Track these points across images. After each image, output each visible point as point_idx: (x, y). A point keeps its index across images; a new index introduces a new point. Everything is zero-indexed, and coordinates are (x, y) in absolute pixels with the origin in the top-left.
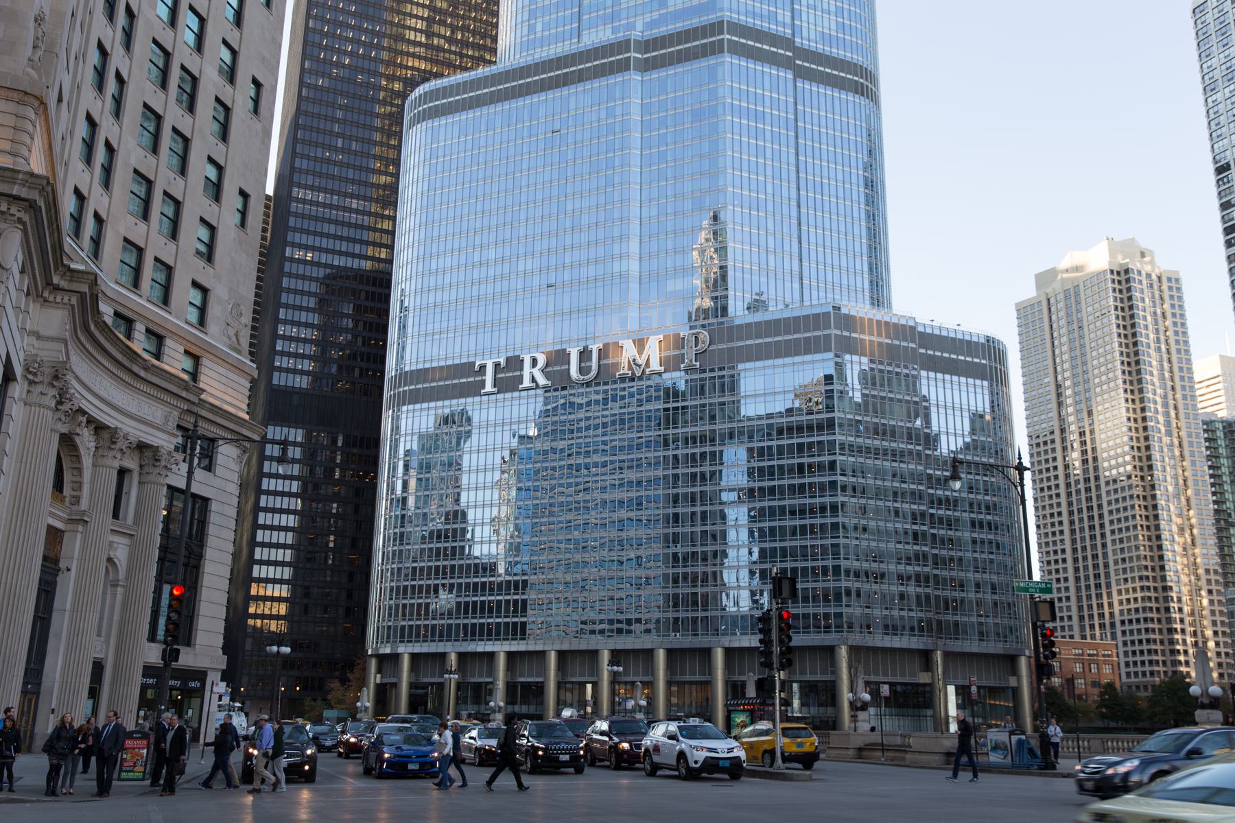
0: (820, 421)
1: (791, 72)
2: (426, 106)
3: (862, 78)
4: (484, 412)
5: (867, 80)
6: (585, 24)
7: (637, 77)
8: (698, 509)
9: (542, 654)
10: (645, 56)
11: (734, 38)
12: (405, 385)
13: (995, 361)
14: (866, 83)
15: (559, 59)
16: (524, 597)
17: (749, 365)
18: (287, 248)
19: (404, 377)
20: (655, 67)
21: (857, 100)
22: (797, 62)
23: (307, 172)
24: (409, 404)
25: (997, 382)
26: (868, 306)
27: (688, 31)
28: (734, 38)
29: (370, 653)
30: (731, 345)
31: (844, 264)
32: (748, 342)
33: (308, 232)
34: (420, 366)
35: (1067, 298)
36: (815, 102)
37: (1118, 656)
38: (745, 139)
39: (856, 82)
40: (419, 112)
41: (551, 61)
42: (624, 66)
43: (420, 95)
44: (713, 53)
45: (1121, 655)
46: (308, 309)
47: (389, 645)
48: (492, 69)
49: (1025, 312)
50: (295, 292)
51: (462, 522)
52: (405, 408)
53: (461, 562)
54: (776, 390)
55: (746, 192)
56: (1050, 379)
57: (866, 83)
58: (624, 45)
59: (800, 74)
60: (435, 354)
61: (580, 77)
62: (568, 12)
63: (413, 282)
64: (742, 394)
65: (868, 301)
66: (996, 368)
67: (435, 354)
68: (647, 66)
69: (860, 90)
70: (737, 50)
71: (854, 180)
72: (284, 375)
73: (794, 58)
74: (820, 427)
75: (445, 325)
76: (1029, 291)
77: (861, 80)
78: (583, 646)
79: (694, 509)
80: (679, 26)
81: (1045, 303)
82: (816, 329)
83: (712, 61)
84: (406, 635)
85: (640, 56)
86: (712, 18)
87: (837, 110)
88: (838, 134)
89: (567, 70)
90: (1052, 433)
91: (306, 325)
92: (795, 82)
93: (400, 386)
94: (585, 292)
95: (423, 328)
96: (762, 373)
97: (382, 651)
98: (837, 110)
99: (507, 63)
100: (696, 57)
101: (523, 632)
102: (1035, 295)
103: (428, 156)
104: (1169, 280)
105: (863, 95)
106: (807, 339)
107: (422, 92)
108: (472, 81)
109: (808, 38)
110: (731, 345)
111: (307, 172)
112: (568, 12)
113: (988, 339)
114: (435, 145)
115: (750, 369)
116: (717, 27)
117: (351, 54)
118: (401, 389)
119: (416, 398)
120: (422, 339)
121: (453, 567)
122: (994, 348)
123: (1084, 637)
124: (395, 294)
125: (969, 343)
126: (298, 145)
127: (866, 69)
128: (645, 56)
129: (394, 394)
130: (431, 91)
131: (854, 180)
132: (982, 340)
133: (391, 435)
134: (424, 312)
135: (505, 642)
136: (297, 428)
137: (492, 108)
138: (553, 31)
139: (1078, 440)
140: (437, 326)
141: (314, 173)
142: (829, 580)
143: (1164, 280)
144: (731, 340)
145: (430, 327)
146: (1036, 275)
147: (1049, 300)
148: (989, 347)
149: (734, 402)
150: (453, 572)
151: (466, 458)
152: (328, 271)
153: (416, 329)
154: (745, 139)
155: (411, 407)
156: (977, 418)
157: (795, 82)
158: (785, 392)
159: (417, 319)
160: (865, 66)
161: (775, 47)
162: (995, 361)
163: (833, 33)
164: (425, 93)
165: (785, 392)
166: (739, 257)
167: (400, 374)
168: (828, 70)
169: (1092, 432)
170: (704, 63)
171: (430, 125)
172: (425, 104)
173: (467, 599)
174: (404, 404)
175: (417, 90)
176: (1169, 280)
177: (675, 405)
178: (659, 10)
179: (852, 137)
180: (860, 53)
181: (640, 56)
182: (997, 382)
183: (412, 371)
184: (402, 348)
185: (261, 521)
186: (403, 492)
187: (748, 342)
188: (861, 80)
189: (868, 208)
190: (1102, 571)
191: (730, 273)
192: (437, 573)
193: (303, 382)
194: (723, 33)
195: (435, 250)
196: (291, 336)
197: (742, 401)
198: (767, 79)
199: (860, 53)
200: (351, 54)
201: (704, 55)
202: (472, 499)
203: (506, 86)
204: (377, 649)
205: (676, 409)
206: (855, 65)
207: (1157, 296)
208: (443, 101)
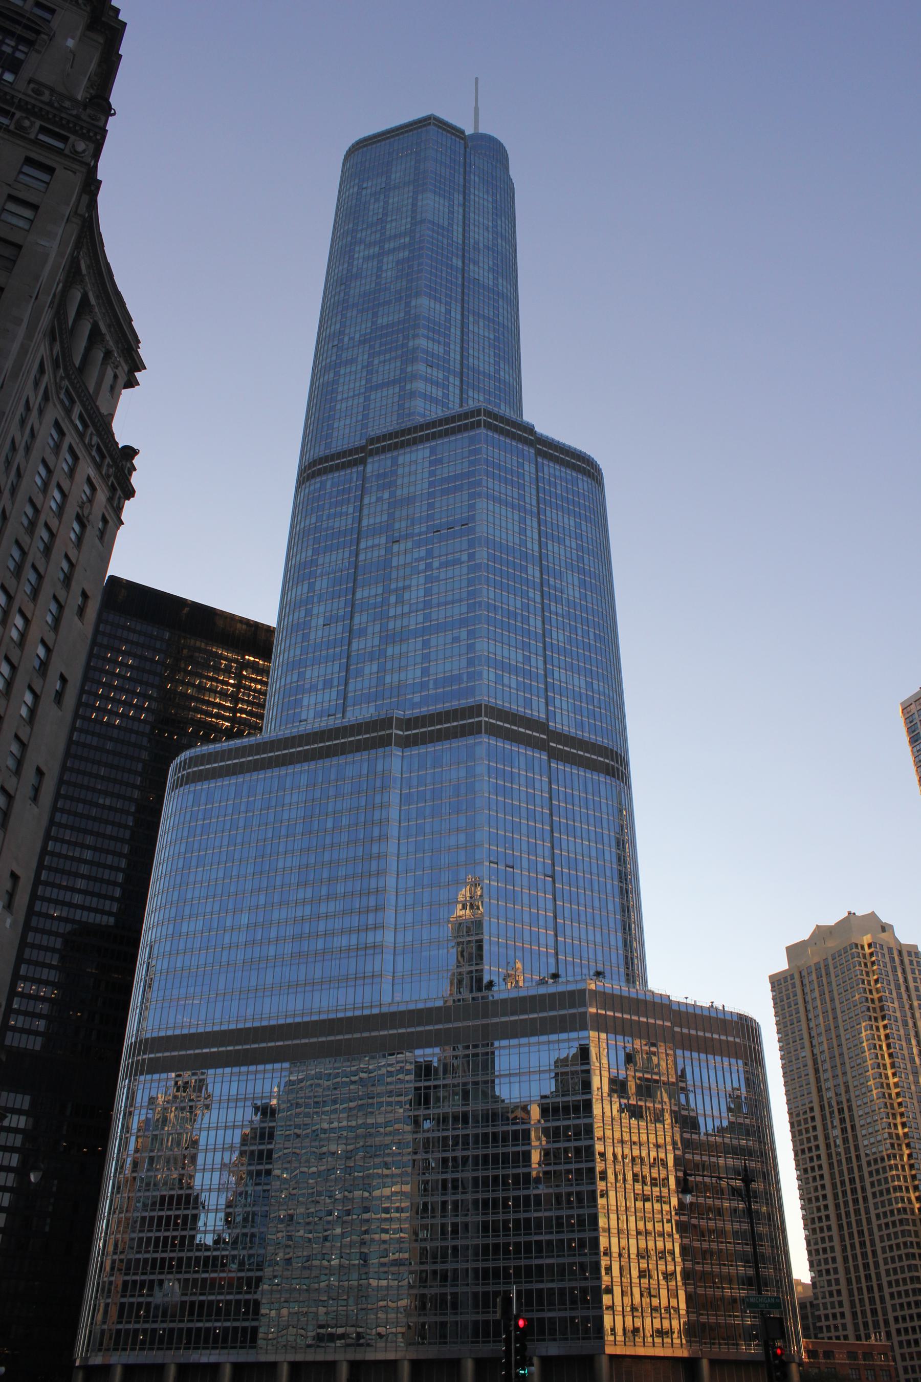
0: (576, 1103)
1: (545, 753)
2: (146, 1056)
3: (612, 760)
4: (226, 1086)
5: (617, 763)
6: (350, 701)
7: (397, 752)
8: (450, 1198)
9: (274, 1365)
10: (406, 733)
11: (491, 721)
12: (145, 1053)
13: (749, 1039)
14: (616, 765)
15: (323, 732)
16: (270, 1147)
17: (504, 1043)
18: (23, 966)
19: (145, 1045)
20: (415, 744)
21: (608, 781)
22: (551, 744)
23: (66, 826)
24: (148, 1073)
25: (752, 1061)
26: (623, 984)
27: (447, 713)
28: (491, 721)
29: (77, 1364)
30: (484, 1021)
31: (598, 939)
32: (504, 1019)
33: (60, 887)
34: (162, 1034)
35: (818, 969)
36: (568, 782)
37: (894, 1360)
38: (501, 815)
39: (608, 764)
40: (183, 775)
41: (316, 733)
42: (384, 742)
43: (185, 760)
44: (471, 733)
45: (898, 1358)
46: (50, 966)
47: (101, 1354)
48: (259, 738)
49: (778, 983)
50: (59, 855)
51: (193, 1208)
52: (142, 1078)
53: (190, 1254)
54: (532, 1070)
55: (501, 832)
56: (807, 1053)
57: (616, 765)
58: (386, 723)
59: (554, 755)
60: (179, 1021)
61: (342, 750)
62: (338, 649)
63: (162, 945)
64: (497, 1073)
65: (623, 978)
66: (750, 1047)
67: (179, 1021)
68: (408, 743)
69: (589, 474)
70: (494, 731)
71: (608, 873)
72: (17, 1035)
73: (549, 740)
74: (576, 1108)
75: (191, 990)
76: (782, 964)
77: (612, 763)
78: (320, 1357)
79: (445, 1198)
80: (440, 707)
81: (797, 976)
82: (572, 1006)
83: (471, 740)
84: (120, 1340)
85: (401, 733)
86: (471, 701)
87: (590, 790)
88: (590, 797)
89: (330, 743)
90: (811, 1102)
91: (47, 983)
92: (549, 762)
93: (139, 1054)
94: (338, 962)
95: (168, 992)
96: (516, 1050)
97: (92, 1362)
98: (590, 790)
99: (273, 734)
100: (455, 736)
101: (254, 1339)
102: (786, 967)
103: (185, 834)
104: (909, 954)
105: (614, 776)
106: (563, 1017)
107: (188, 757)
108: (237, 749)
109: (563, 723)
110: (484, 1021)
111: (66, 826)
112: (338, 649)
113: (740, 1016)
114: (195, 809)
115: (504, 1047)
116: (475, 710)
117: (123, 716)
118: (140, 1058)
119: (155, 1067)
120: (166, 1004)
121: (180, 1260)
122: (747, 1026)
123: (858, 1338)
124: (143, 955)
125: (724, 1021)
126: (75, 733)
127: (617, 753)
128: (406, 733)
129: (133, 1063)
130: (197, 756)
131: (608, 873)
132: (735, 1019)
133: (126, 1107)
134: (171, 976)
135: (232, 1351)
136: (24, 1094)
137: (255, 776)
138: (324, 653)
139: (840, 1137)
140: (183, 991)
141: (72, 828)
142: (585, 1254)
143: (905, 954)
144: (485, 1016)
145: (175, 992)
146: (787, 948)
147: (800, 973)
148: (742, 1025)
149: (487, 1054)
150: (179, 1265)
151: (198, 1176)
152: (75, 926)
153: (161, 993)
154: (501, 815)
155: (149, 1077)
156: (735, 1098)
157: (549, 762)
158: (540, 1072)
159: (163, 983)
160: (615, 749)
161: (530, 730)
162: (749, 1039)
163: (583, 691)
164: (191, 758)
165: (540, 1072)
166: (494, 931)
167: (141, 1041)
168: (581, 753)
169: (850, 1109)
170: (463, 742)
171: (192, 789)
172: (189, 768)
173: (193, 1298)
174: (142, 1074)
175: (183, 755)
176: (909, 954)
177: (427, 1084)
178: (420, 692)
179: (605, 816)
180: (610, 738)
181: (401, 733)
182: (752, 1061)
183: (153, 1039)
184: (144, 1007)
185: (37, 908)
186: (133, 1171)
187: (504, 1019)
188: (612, 763)
189: (621, 884)
190: (871, 1260)
191: (486, 947)
192: (165, 1245)
193: (35, 1044)
194: (481, 716)
195: (182, 946)
196: (30, 994)
197: (497, 1053)
198: (522, 759)
199: (610, 738)
200: (123, 716)
201: (463, 735)
202: (207, 1182)
203: (270, 755)
204: (86, 1358)
205: (428, 1088)
206: (606, 748)
207: (907, 1007)
208: (208, 766)
